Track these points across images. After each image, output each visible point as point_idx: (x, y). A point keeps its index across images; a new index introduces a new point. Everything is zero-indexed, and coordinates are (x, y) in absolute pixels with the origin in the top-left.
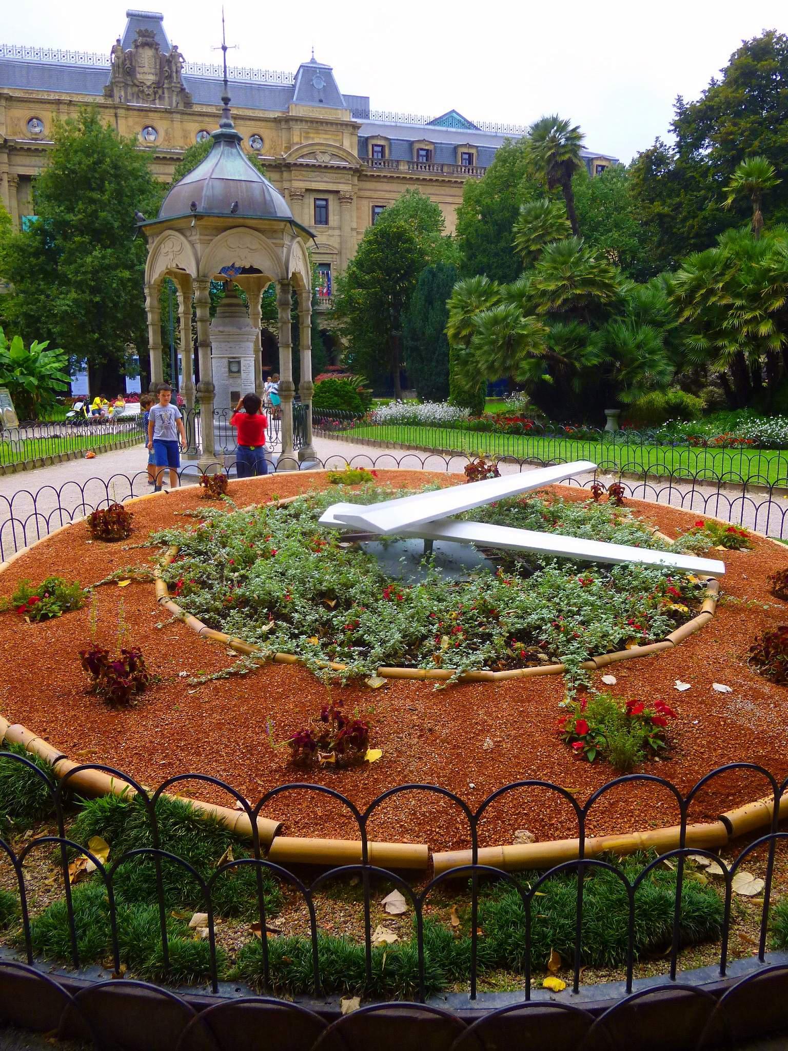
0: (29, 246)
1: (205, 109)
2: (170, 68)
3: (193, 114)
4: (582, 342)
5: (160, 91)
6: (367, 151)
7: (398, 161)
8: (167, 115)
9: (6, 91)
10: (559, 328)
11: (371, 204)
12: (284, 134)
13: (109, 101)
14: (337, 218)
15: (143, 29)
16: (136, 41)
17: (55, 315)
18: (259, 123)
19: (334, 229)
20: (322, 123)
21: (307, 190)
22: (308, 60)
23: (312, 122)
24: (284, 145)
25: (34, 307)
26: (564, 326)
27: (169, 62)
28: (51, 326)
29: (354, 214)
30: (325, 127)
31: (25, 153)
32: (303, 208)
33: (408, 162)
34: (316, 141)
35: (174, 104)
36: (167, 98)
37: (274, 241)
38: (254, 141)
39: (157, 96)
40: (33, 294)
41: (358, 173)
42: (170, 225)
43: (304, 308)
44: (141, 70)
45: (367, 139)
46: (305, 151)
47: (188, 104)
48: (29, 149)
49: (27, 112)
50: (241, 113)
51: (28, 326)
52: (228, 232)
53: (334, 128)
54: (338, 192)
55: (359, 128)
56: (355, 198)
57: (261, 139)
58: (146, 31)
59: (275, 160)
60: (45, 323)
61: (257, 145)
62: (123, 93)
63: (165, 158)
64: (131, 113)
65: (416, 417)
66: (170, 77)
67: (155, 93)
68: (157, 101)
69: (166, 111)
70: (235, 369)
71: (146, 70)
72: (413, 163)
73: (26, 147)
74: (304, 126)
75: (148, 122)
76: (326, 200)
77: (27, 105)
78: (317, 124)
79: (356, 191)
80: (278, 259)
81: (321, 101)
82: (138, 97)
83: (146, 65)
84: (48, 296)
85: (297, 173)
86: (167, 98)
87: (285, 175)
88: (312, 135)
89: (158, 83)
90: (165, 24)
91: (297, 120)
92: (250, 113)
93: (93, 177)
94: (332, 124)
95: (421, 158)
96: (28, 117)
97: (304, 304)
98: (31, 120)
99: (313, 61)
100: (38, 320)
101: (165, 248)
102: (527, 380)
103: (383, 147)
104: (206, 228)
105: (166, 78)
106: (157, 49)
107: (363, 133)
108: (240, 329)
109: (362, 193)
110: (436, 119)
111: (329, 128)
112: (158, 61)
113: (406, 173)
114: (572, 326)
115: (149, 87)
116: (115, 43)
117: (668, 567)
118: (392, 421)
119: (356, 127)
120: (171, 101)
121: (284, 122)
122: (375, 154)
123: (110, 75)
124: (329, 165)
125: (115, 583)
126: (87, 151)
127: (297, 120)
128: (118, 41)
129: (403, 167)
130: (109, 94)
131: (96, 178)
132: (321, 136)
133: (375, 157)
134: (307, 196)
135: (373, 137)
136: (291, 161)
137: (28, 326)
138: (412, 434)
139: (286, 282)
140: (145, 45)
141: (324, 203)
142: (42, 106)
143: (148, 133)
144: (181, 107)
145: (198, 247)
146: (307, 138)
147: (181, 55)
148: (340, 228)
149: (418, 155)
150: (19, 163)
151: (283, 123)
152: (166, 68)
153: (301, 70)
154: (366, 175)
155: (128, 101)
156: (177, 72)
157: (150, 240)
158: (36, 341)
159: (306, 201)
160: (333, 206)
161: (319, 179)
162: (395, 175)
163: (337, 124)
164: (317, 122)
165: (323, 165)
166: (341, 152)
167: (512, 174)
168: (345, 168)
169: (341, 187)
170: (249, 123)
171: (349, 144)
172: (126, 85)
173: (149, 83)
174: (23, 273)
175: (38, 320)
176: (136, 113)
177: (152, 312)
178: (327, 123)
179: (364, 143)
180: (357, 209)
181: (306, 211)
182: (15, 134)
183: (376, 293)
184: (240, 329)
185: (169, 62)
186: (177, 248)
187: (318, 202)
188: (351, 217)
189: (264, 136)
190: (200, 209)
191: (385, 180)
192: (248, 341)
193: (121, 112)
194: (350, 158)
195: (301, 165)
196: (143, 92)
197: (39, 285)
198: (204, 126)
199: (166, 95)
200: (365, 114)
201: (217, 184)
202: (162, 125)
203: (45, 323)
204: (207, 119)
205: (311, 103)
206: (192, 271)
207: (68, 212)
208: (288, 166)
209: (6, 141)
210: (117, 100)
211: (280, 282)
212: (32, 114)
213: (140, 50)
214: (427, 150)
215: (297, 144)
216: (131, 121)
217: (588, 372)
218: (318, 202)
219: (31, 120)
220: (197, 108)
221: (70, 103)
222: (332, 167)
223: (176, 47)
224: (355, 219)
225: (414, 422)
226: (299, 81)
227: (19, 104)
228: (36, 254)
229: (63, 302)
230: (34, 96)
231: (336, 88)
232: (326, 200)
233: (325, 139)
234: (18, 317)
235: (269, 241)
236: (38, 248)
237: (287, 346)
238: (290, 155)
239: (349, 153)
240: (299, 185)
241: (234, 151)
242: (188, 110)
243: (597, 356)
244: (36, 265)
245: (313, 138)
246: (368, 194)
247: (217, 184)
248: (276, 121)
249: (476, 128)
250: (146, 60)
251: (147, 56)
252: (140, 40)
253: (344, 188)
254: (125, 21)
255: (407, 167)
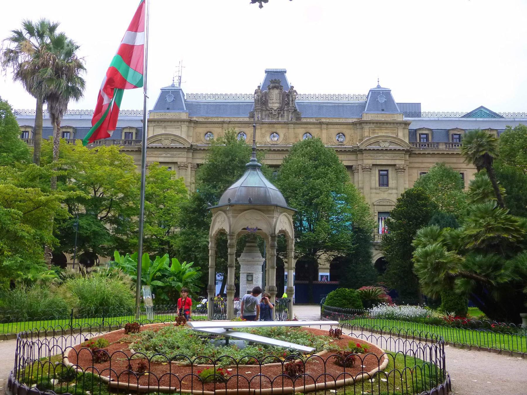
0: (191, 207)
1: (308, 120)
2: (288, 99)
3: (301, 124)
4: (497, 267)
5: (282, 112)
6: (416, 138)
7: (438, 143)
8: (285, 125)
9: (194, 119)
10: (479, 258)
11: (419, 172)
12: (359, 132)
13: (252, 120)
14: (394, 182)
15: (273, 79)
16: (269, 86)
17: (200, 247)
18: (342, 126)
19: (392, 189)
20: (383, 123)
21: (373, 165)
22: (376, 86)
23: (377, 123)
24: (359, 138)
25: (189, 242)
26: (484, 257)
27: (288, 95)
28: (196, 254)
29: (407, 179)
30: (385, 125)
31: (202, 152)
32: (371, 177)
33: (446, 143)
34: (380, 134)
35: (290, 119)
36: (286, 116)
37: (268, 215)
38: (339, 137)
39: (280, 115)
40: (189, 235)
41: (410, 153)
42: (222, 209)
43: (290, 248)
44: (271, 102)
45: (416, 131)
46: (372, 141)
47: (298, 118)
48: (204, 150)
49: (205, 129)
50: (331, 121)
51: (185, 253)
52: (245, 212)
53: (392, 126)
54: (395, 165)
55: (409, 124)
56: (407, 169)
57: (344, 136)
58: (275, 80)
59: (352, 148)
60: (194, 252)
61: (341, 139)
62: (260, 115)
63: (283, 150)
64: (264, 125)
65: (393, 314)
66: (288, 104)
67: (279, 114)
68: (280, 118)
69: (286, 123)
70: (250, 279)
71: (274, 101)
72: (449, 144)
73: (202, 148)
74: (372, 125)
75: (274, 130)
76: (387, 171)
77: (205, 125)
78: (380, 124)
79: (408, 163)
80: (270, 224)
81: (383, 110)
82: (269, 116)
83: (274, 98)
84: (197, 236)
85: (367, 155)
86: (286, 116)
87: (359, 156)
88: (377, 131)
89: (281, 108)
90: (287, 75)
91: (367, 123)
92: (337, 121)
93: (229, 169)
94: (390, 123)
95: (455, 140)
96: (206, 132)
97: (290, 246)
98: (207, 133)
99: (379, 87)
100: (190, 250)
101: (218, 219)
102: (462, 292)
103: (427, 135)
104: (235, 210)
105: (286, 104)
106: (281, 89)
107: (413, 127)
108: (253, 258)
109: (412, 165)
110: (468, 114)
111: (388, 126)
112: (281, 95)
113: (446, 150)
114: (490, 255)
115: (275, 111)
116: (257, 88)
117: (291, 348)
118: (379, 317)
119: (407, 124)
120: (288, 117)
121: (360, 124)
122: (422, 140)
123: (254, 106)
124: (389, 149)
125: (120, 343)
126: (227, 154)
127: (367, 123)
128: (259, 87)
129: (442, 147)
130: (252, 116)
131: (230, 169)
132: (383, 131)
133: (422, 141)
134: (374, 168)
135: (420, 129)
136: (363, 147)
137: (185, 253)
138: (389, 325)
139: (273, 235)
140: (274, 88)
141: (385, 172)
142: (213, 125)
143: (274, 137)
144: (294, 121)
145: (231, 219)
146: (374, 133)
147: (295, 91)
148: (397, 189)
149: (453, 139)
150: (199, 157)
151: (358, 125)
152: (286, 99)
153: (370, 93)
154: (415, 154)
155: (263, 119)
156: (292, 101)
157: (213, 216)
158: (185, 262)
159: (373, 171)
160: (392, 174)
161: (381, 157)
162: (436, 152)
163: (394, 123)
164: (380, 123)
165: (384, 149)
166: (397, 140)
167: (512, 149)
168: (399, 150)
169: (397, 162)
170: (336, 126)
171: (403, 135)
172: (262, 110)
173: (275, 109)
174: (185, 223)
175: (190, 250)
176: (266, 125)
177: (211, 249)
178: (387, 123)
179: (413, 134)
180: (409, 175)
181: (373, 178)
182: (197, 141)
183: (401, 234)
184: (253, 258)
185: (288, 95)
186: (223, 220)
187: (381, 172)
188: (405, 181)
189: (345, 134)
190: (232, 202)
191: (430, 156)
192: (257, 265)
193: (258, 126)
194: (403, 143)
195: (370, 150)
196: (272, 113)
197: (194, 229)
198: (308, 130)
199: (285, 114)
200: (418, 114)
201: (243, 189)
202: (282, 132)
203: (194, 252)
204: (310, 126)
205: (377, 112)
206: (227, 230)
207: (213, 188)
208: (361, 151)
209: (192, 145)
210: (256, 119)
211: (272, 237)
212: (208, 130)
213: (271, 91)
214: (460, 135)
215: (367, 137)
216: (263, 131)
217: (503, 287)
218: (381, 172)
219: (207, 133)
220: (304, 120)
221: (230, 123)
222: (391, 150)
223: (292, 87)
224: (407, 182)
225: (391, 317)
226: (369, 99)
227: (201, 125)
228: (194, 212)
229: (204, 239)
230: (210, 120)
231: (393, 101)
232: (387, 171)
233: (386, 133)
234: (180, 248)
235: (266, 216)
236: (195, 209)
237: (273, 268)
238: (362, 144)
239: (402, 141)
240: (368, 162)
241: (255, 172)
242: (298, 122)
243: (509, 276)
244: (193, 218)
245: (378, 133)
246: (417, 165)
247: (243, 189)
248: (354, 124)
249: (502, 117)
250: (275, 96)
251: (275, 93)
252: (272, 85)
253: (399, 162)
254: (263, 76)
255: (444, 146)
